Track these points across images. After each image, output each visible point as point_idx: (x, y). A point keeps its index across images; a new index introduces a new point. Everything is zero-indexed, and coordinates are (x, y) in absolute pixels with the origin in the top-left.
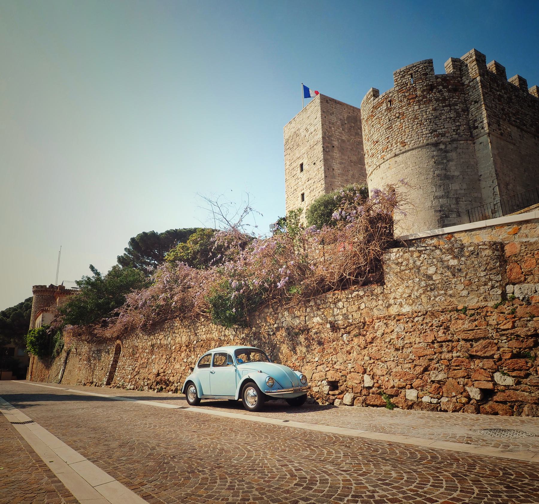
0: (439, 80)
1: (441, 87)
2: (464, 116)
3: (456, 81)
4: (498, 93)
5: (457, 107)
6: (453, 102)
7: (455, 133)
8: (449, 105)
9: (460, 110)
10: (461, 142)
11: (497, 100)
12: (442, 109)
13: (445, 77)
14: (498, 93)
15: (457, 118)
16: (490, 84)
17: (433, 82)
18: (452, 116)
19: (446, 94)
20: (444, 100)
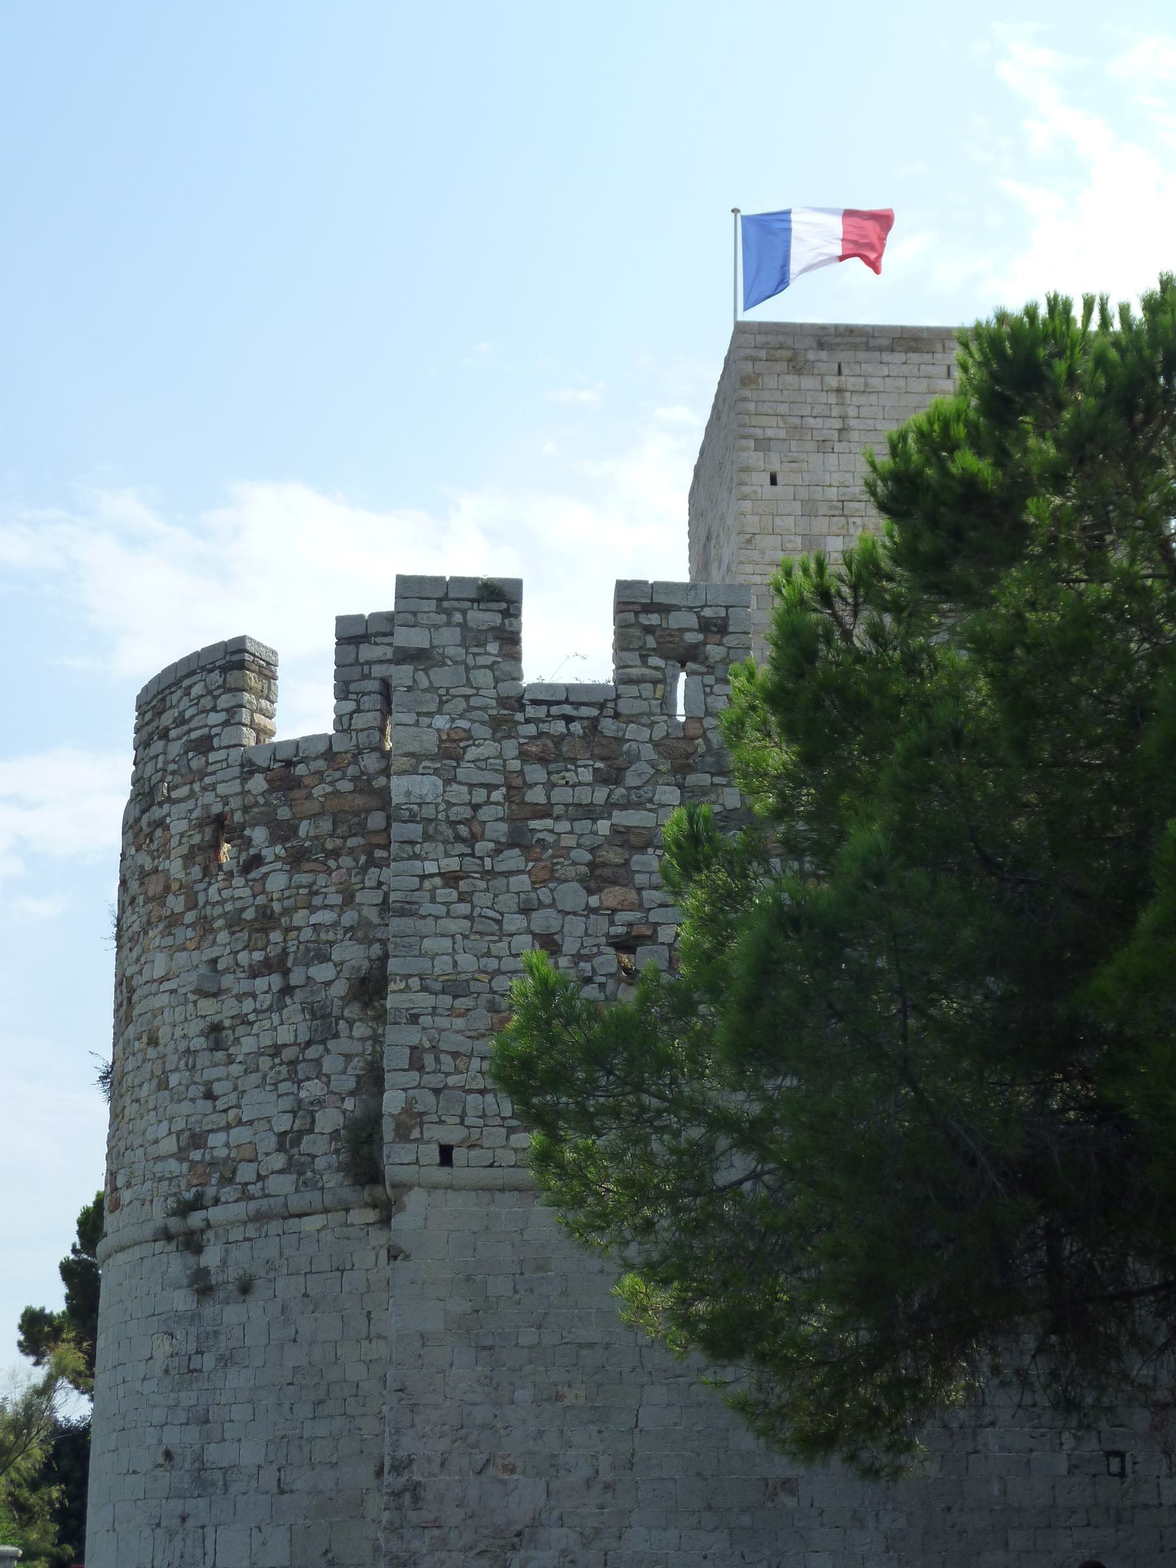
0: (258, 783)
1: (259, 835)
2: (360, 1030)
3: (345, 786)
4: (603, 827)
5: (322, 972)
6: (307, 934)
7: (279, 1161)
8: (277, 965)
9: (340, 989)
10: (310, 1224)
11: (572, 895)
12: (245, 986)
13: (289, 764)
14: (603, 827)
15: (313, 1052)
16: (515, 789)
17: (225, 800)
18: (284, 1035)
19: (277, 882)
20: (266, 920)
